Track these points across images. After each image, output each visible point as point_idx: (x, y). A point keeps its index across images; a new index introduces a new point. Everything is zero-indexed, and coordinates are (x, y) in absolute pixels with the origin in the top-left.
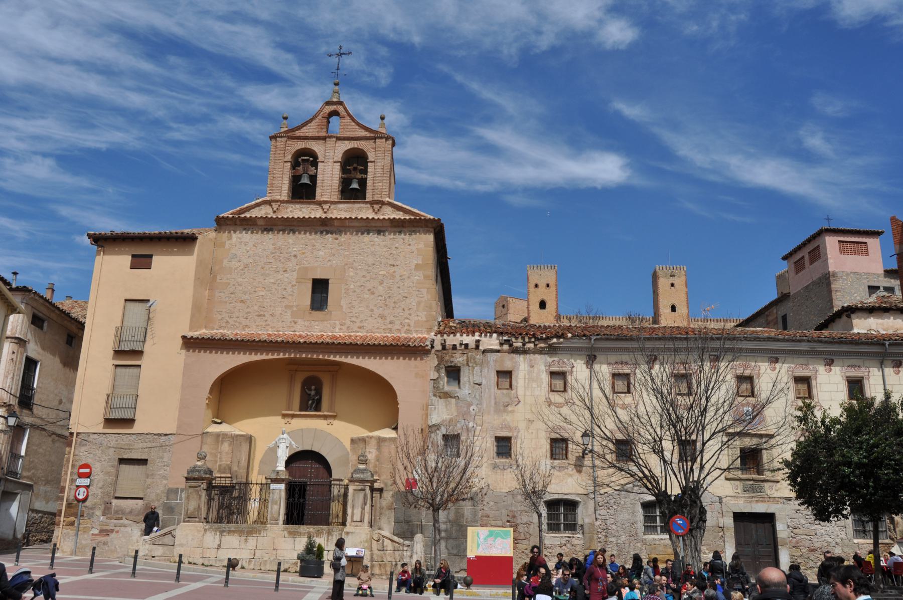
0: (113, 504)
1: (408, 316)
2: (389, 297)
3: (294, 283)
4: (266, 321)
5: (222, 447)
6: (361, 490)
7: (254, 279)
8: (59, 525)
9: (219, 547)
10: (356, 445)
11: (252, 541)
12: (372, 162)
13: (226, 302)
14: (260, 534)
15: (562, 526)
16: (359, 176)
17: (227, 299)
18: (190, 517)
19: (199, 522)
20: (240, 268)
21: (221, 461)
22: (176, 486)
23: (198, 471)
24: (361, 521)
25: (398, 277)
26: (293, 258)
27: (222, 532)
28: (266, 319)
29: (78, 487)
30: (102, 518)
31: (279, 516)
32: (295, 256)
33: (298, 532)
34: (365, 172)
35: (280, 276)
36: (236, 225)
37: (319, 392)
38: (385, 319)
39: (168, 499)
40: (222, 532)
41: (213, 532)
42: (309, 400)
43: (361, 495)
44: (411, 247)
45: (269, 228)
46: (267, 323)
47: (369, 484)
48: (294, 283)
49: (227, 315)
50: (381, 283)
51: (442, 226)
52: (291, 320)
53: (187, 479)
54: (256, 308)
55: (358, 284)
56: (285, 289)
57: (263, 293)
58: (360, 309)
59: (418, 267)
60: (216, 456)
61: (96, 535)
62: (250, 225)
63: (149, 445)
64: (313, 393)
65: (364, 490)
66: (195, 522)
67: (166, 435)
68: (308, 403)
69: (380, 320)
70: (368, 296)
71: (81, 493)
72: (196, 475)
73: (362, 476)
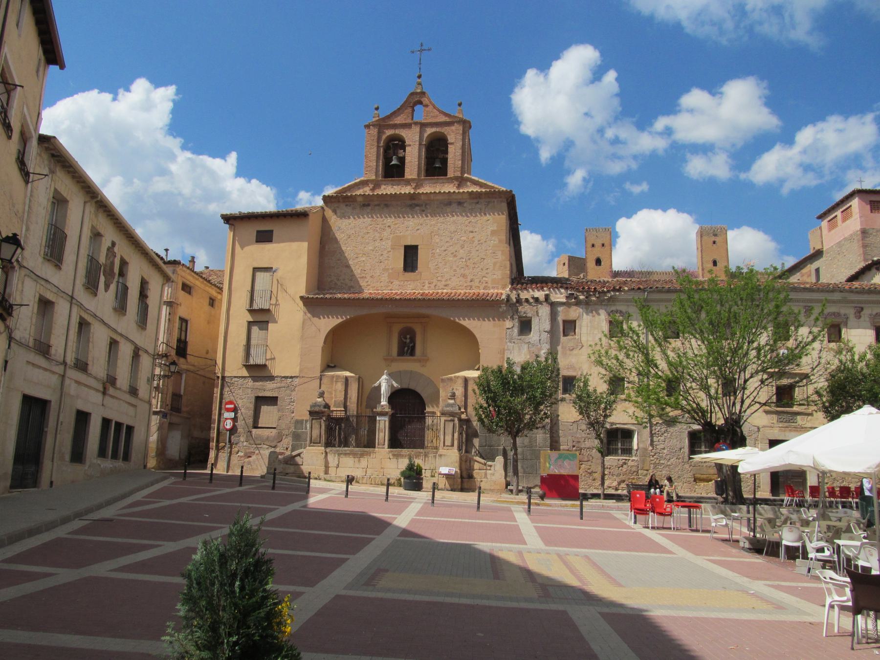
1: (487, 275)
2: (469, 259)
3: (390, 249)
4: (367, 282)
8: (213, 449)
9: (338, 466)
10: (445, 384)
11: (364, 462)
12: (452, 144)
14: (370, 456)
15: (620, 451)
18: (313, 442)
19: (321, 446)
20: (345, 238)
21: (336, 398)
22: (300, 418)
23: (319, 406)
24: (451, 446)
25: (476, 242)
26: (387, 228)
27: (339, 455)
28: (366, 280)
29: (226, 419)
30: (245, 444)
32: (389, 226)
33: (401, 455)
35: (377, 244)
36: (339, 202)
37: (413, 340)
38: (467, 278)
39: (295, 428)
40: (339, 455)
41: (333, 455)
42: (405, 347)
43: (451, 424)
45: (366, 203)
48: (390, 249)
50: (462, 247)
51: (513, 197)
53: (311, 413)
55: (443, 248)
56: (382, 255)
57: (364, 259)
59: (493, 233)
60: (332, 394)
61: (241, 457)
62: (352, 202)
63: (279, 385)
64: (408, 341)
65: (453, 421)
66: (319, 446)
67: (291, 377)
68: (404, 349)
69: (461, 278)
70: (451, 259)
71: (228, 424)
72: (317, 409)
73: (451, 409)
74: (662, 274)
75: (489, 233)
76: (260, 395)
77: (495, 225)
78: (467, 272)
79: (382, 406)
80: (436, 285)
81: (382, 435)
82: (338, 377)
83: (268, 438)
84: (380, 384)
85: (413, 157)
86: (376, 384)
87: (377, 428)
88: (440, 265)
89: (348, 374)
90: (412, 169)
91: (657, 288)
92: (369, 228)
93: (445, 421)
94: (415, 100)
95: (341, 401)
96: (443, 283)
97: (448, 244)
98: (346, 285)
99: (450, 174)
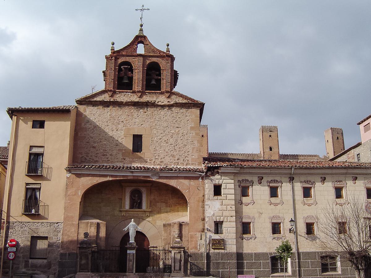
0: (30, 262)
1: (188, 156)
2: (176, 145)
4: (108, 158)
5: (90, 230)
6: (179, 252)
7: (100, 135)
13: (84, 148)
15: (329, 269)
16: (156, 77)
17: (85, 145)
25: (181, 135)
26: (121, 123)
31: (133, 268)
32: (122, 122)
34: (160, 75)
44: (187, 117)
46: (108, 159)
47: (183, 250)
48: (123, 137)
49: (85, 155)
50: (172, 137)
52: (122, 158)
54: (102, 151)
55: (159, 137)
57: (105, 143)
58: (161, 152)
59: (192, 128)
64: (136, 199)
68: (134, 204)
69: (171, 158)
74: (237, 155)
75: (189, 128)
76: (35, 235)
77: (193, 123)
78: (175, 153)
79: (131, 243)
80: (154, 162)
81: (131, 263)
82: (92, 223)
83: (40, 266)
84: (128, 228)
85: (138, 76)
86: (126, 229)
87: (128, 258)
88: (157, 148)
89: (98, 221)
90: (137, 85)
91: (263, 166)
92: (109, 122)
93: (175, 253)
94: (140, 39)
95: (94, 240)
96: (160, 160)
97: (162, 135)
98: (93, 159)
99: (163, 89)
